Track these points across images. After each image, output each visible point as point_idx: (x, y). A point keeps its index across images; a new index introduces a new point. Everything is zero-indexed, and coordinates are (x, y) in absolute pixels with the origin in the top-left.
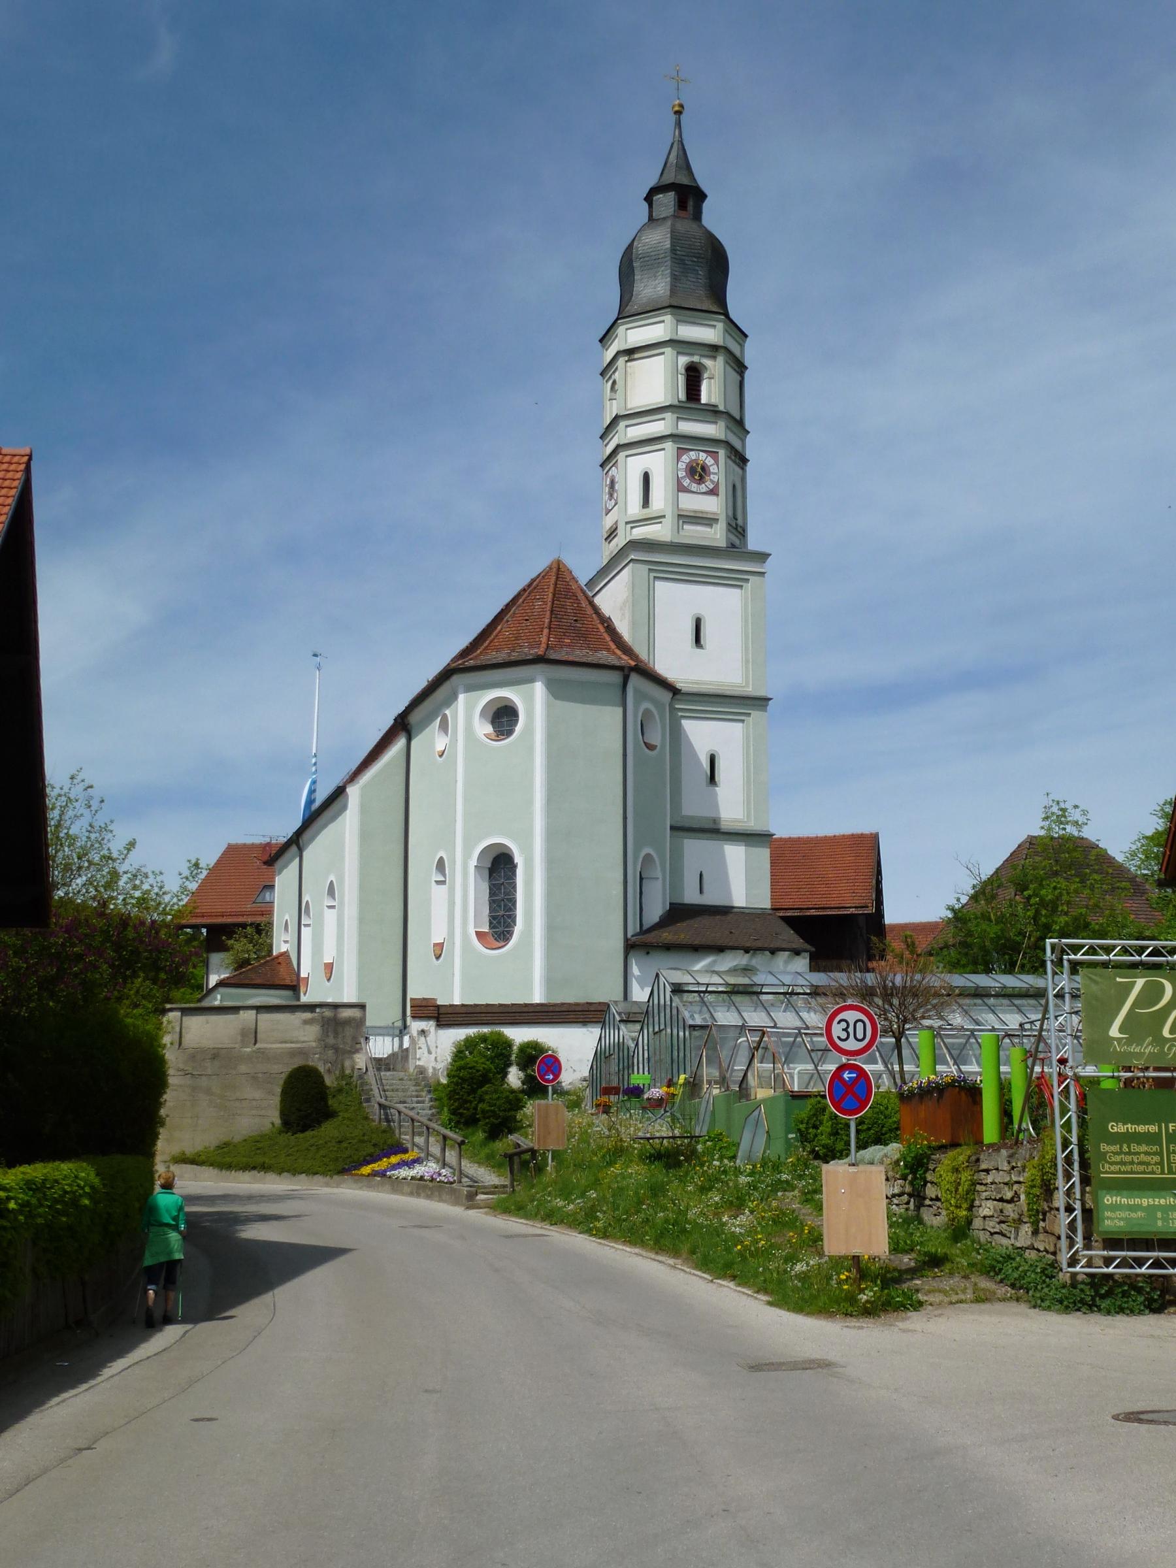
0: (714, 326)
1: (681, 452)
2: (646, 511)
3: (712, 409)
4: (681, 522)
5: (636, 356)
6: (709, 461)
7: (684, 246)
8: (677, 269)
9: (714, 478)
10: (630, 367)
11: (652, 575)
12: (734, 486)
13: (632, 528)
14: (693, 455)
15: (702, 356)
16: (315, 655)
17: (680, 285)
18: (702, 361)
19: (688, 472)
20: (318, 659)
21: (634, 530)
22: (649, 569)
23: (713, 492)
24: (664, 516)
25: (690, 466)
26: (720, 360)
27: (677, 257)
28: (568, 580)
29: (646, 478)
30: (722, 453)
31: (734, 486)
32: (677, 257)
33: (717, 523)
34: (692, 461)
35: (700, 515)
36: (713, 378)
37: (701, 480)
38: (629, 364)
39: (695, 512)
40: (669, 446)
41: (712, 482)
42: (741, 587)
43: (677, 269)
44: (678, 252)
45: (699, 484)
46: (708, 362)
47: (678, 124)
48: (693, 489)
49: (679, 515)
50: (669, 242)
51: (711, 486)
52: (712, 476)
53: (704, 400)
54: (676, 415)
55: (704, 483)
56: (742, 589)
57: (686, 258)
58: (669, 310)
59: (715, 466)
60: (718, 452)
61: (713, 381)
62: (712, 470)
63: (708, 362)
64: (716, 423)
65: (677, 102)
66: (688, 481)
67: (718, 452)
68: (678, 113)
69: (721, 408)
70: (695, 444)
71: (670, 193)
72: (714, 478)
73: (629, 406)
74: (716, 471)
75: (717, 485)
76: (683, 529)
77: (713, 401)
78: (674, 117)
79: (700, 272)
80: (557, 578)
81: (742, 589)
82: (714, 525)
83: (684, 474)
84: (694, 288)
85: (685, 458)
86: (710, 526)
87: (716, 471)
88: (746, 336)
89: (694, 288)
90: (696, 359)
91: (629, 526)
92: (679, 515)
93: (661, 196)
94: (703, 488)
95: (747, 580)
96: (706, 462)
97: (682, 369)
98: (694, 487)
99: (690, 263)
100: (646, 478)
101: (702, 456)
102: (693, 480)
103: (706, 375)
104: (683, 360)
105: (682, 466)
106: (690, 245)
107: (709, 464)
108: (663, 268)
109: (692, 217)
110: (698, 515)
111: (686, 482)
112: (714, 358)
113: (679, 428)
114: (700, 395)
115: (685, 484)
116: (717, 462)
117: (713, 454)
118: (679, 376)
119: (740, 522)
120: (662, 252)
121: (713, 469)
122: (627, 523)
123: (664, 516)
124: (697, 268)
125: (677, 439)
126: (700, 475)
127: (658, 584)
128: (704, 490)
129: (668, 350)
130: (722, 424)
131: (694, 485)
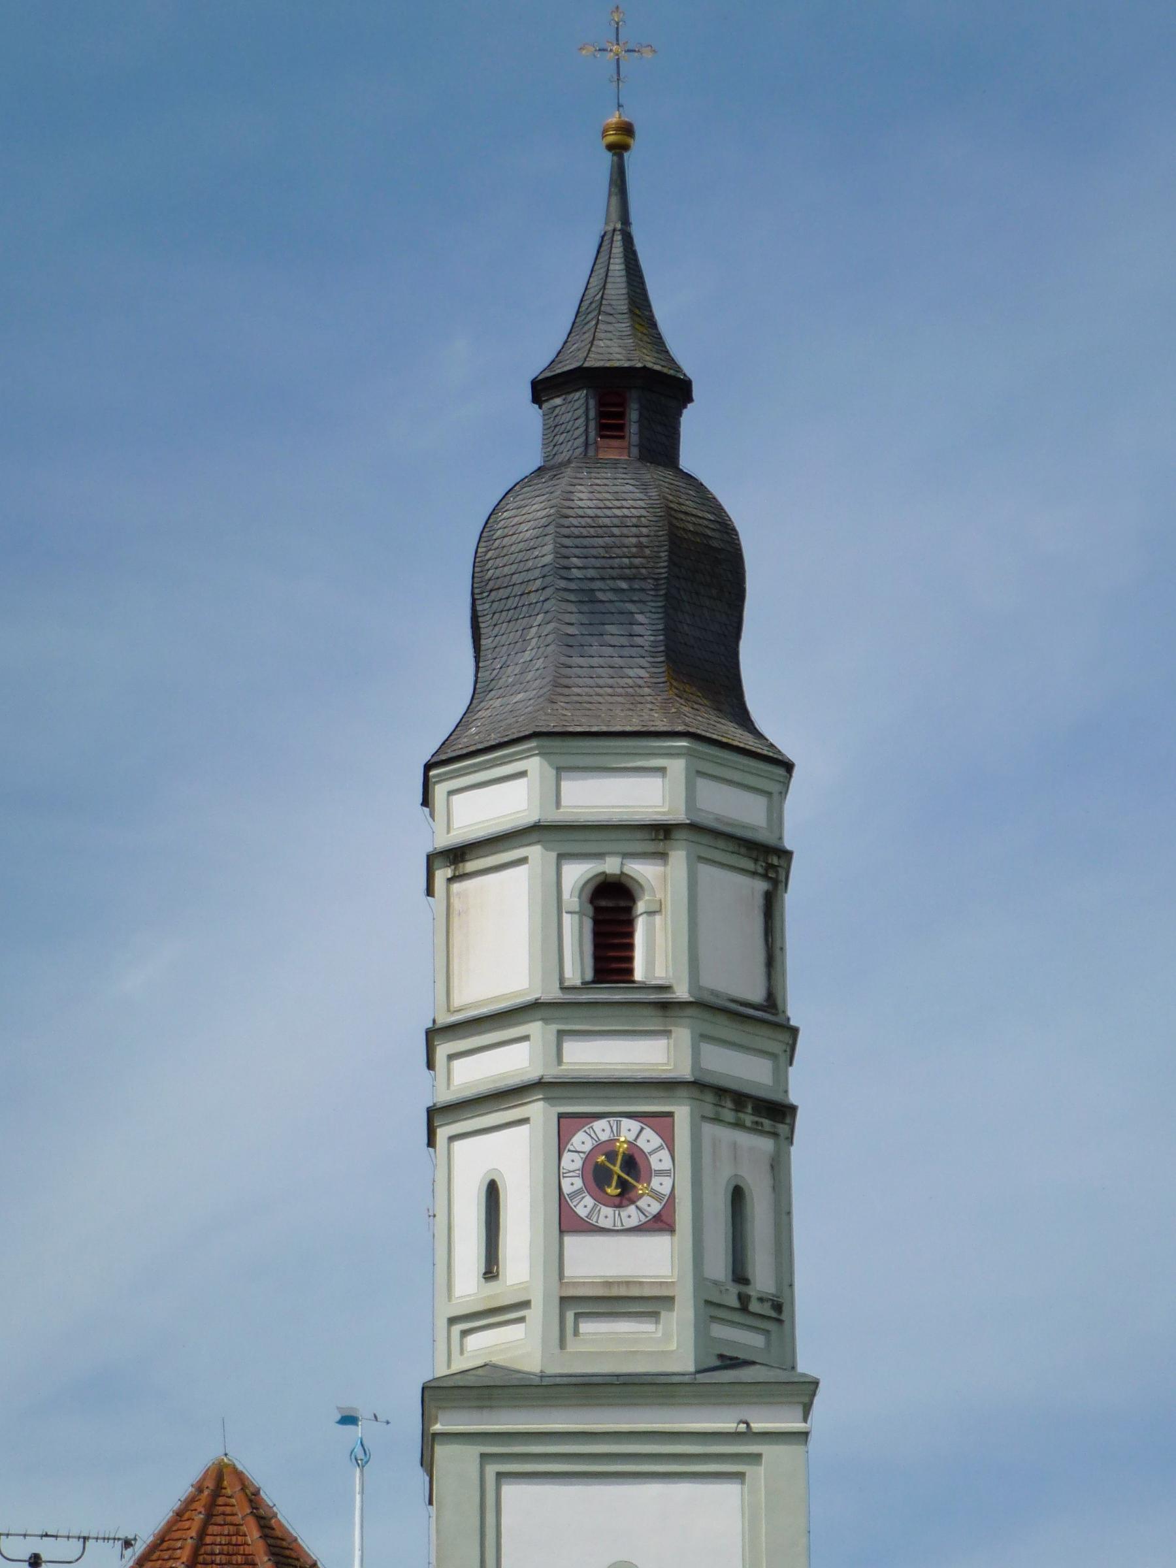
0: (662, 770)
1: (567, 1125)
2: (493, 1287)
3: (653, 997)
4: (570, 1316)
5: (470, 866)
6: (649, 1140)
7: (594, 552)
8: (572, 618)
9: (662, 1185)
10: (458, 894)
11: (492, 1469)
12: (738, 1196)
13: (465, 1333)
14: (602, 1129)
15: (626, 855)
16: (349, 1420)
17: (581, 661)
18: (626, 870)
19: (590, 1177)
20: (358, 1431)
21: (473, 1341)
22: (483, 1456)
23: (661, 1223)
24: (526, 1304)
25: (590, 1168)
26: (679, 857)
27: (573, 586)
28: (237, 1519)
29: (492, 1192)
30: (682, 1113)
31: (738, 1196)
32: (573, 586)
33: (671, 1309)
34: (599, 1147)
35: (623, 1292)
36: (659, 912)
37: (626, 1195)
38: (456, 887)
39: (608, 1284)
40: (537, 1110)
41: (657, 1196)
42: (740, 1476)
43: (572, 618)
44: (576, 573)
45: (619, 1206)
46: (643, 871)
47: (619, 182)
48: (603, 1223)
49: (563, 1299)
50: (549, 548)
51: (655, 1208)
52: (655, 1182)
53: (639, 975)
54: (554, 1027)
55: (632, 1202)
56: (743, 1483)
57: (598, 584)
58: (533, 744)
59: (665, 1154)
60: (670, 1115)
61: (658, 918)
62: (655, 1165)
63: (643, 871)
64: (667, 1033)
65: (614, 119)
66: (589, 1201)
67: (670, 1115)
68: (618, 149)
69: (682, 993)
70: (607, 1099)
71: (577, 395)
72: (662, 1185)
73: (457, 1001)
74: (667, 1164)
75: (670, 1202)
76: (576, 1333)
77: (661, 975)
78: (608, 158)
79: (640, 618)
80: (209, 1516)
81: (743, 1483)
82: (664, 1314)
83: (579, 1183)
84: (618, 661)
85: (582, 1141)
86: (654, 1315)
87: (667, 1164)
88: (788, 767)
89: (618, 661)
90: (611, 866)
91: (457, 1328)
92: (563, 1299)
93: (558, 401)
94: (631, 1216)
95: (756, 1458)
96: (640, 1143)
97: (571, 899)
98: (606, 1216)
99: (610, 596)
100: (492, 1192)
101: (629, 1128)
102: (602, 1199)
103: (641, 907)
104: (577, 874)
105: (572, 1162)
106: (605, 547)
107: (647, 1148)
108: (540, 617)
109: (635, 451)
110: (615, 1292)
111: (584, 1207)
112: (662, 856)
113: (566, 1058)
114: (630, 959)
115: (582, 1211)
116: (669, 1143)
117: (661, 1122)
118: (567, 918)
119: (762, 1280)
120: (537, 573)
121: (659, 1160)
122: (452, 1321)
123: (526, 1304)
124: (631, 607)
125: (557, 1092)
126: (624, 1186)
127: (510, 1491)
128: (634, 1222)
129: (534, 852)
130: (683, 1034)
131: (607, 1211)
